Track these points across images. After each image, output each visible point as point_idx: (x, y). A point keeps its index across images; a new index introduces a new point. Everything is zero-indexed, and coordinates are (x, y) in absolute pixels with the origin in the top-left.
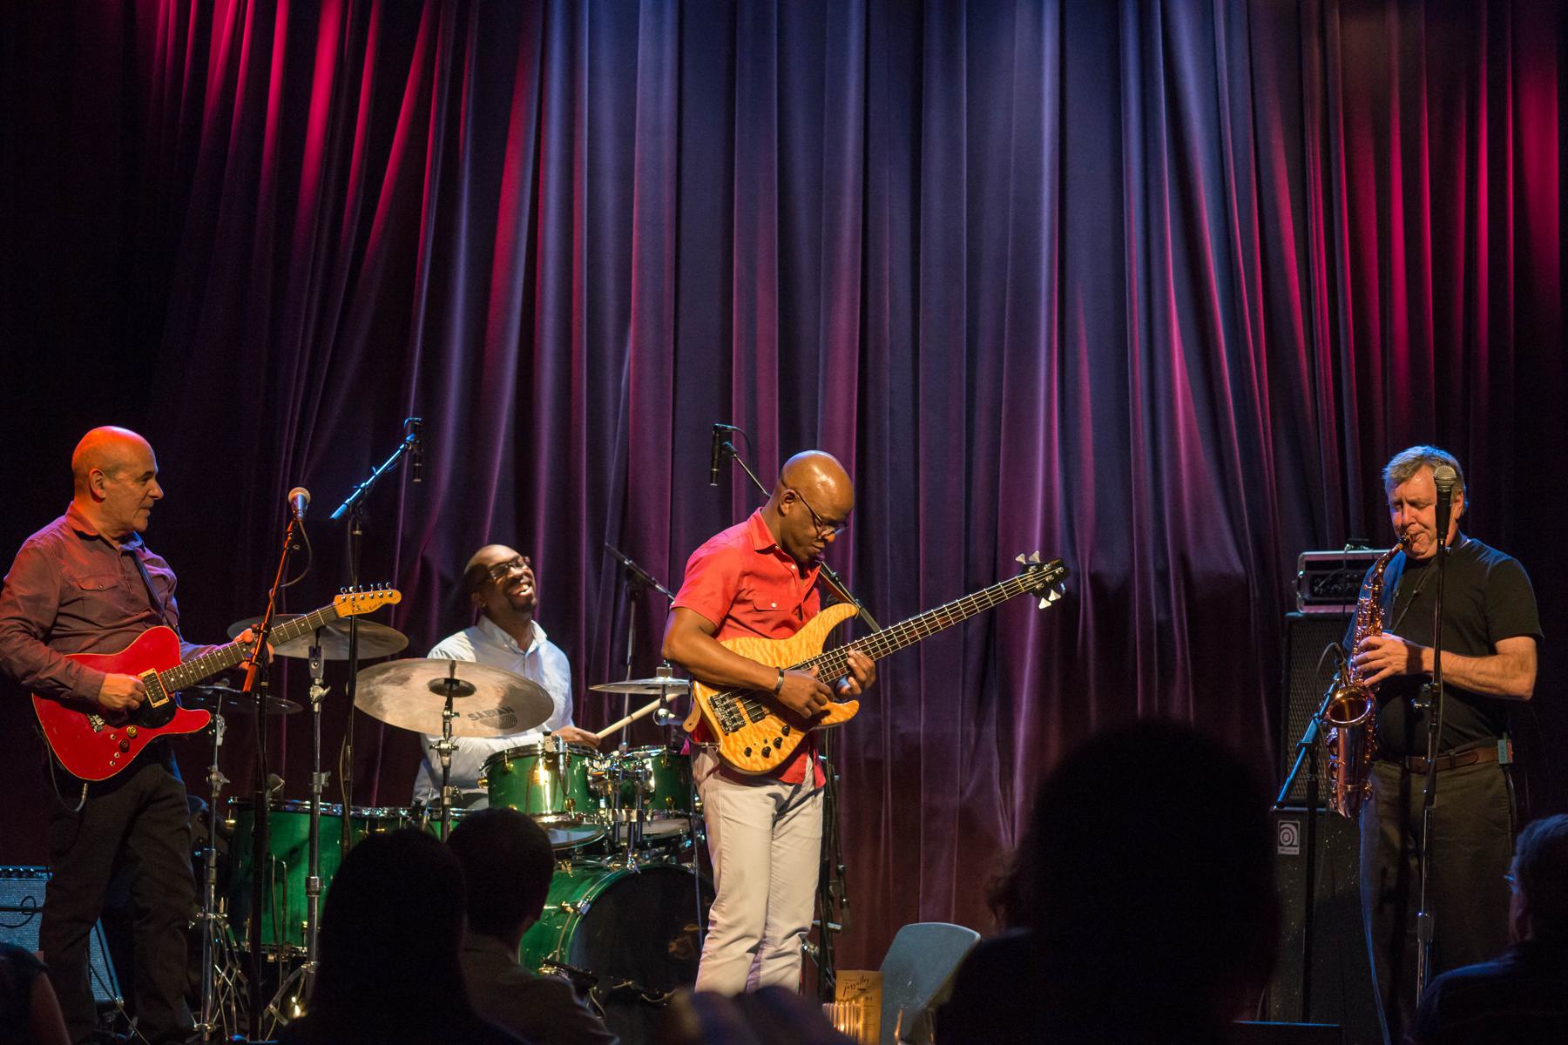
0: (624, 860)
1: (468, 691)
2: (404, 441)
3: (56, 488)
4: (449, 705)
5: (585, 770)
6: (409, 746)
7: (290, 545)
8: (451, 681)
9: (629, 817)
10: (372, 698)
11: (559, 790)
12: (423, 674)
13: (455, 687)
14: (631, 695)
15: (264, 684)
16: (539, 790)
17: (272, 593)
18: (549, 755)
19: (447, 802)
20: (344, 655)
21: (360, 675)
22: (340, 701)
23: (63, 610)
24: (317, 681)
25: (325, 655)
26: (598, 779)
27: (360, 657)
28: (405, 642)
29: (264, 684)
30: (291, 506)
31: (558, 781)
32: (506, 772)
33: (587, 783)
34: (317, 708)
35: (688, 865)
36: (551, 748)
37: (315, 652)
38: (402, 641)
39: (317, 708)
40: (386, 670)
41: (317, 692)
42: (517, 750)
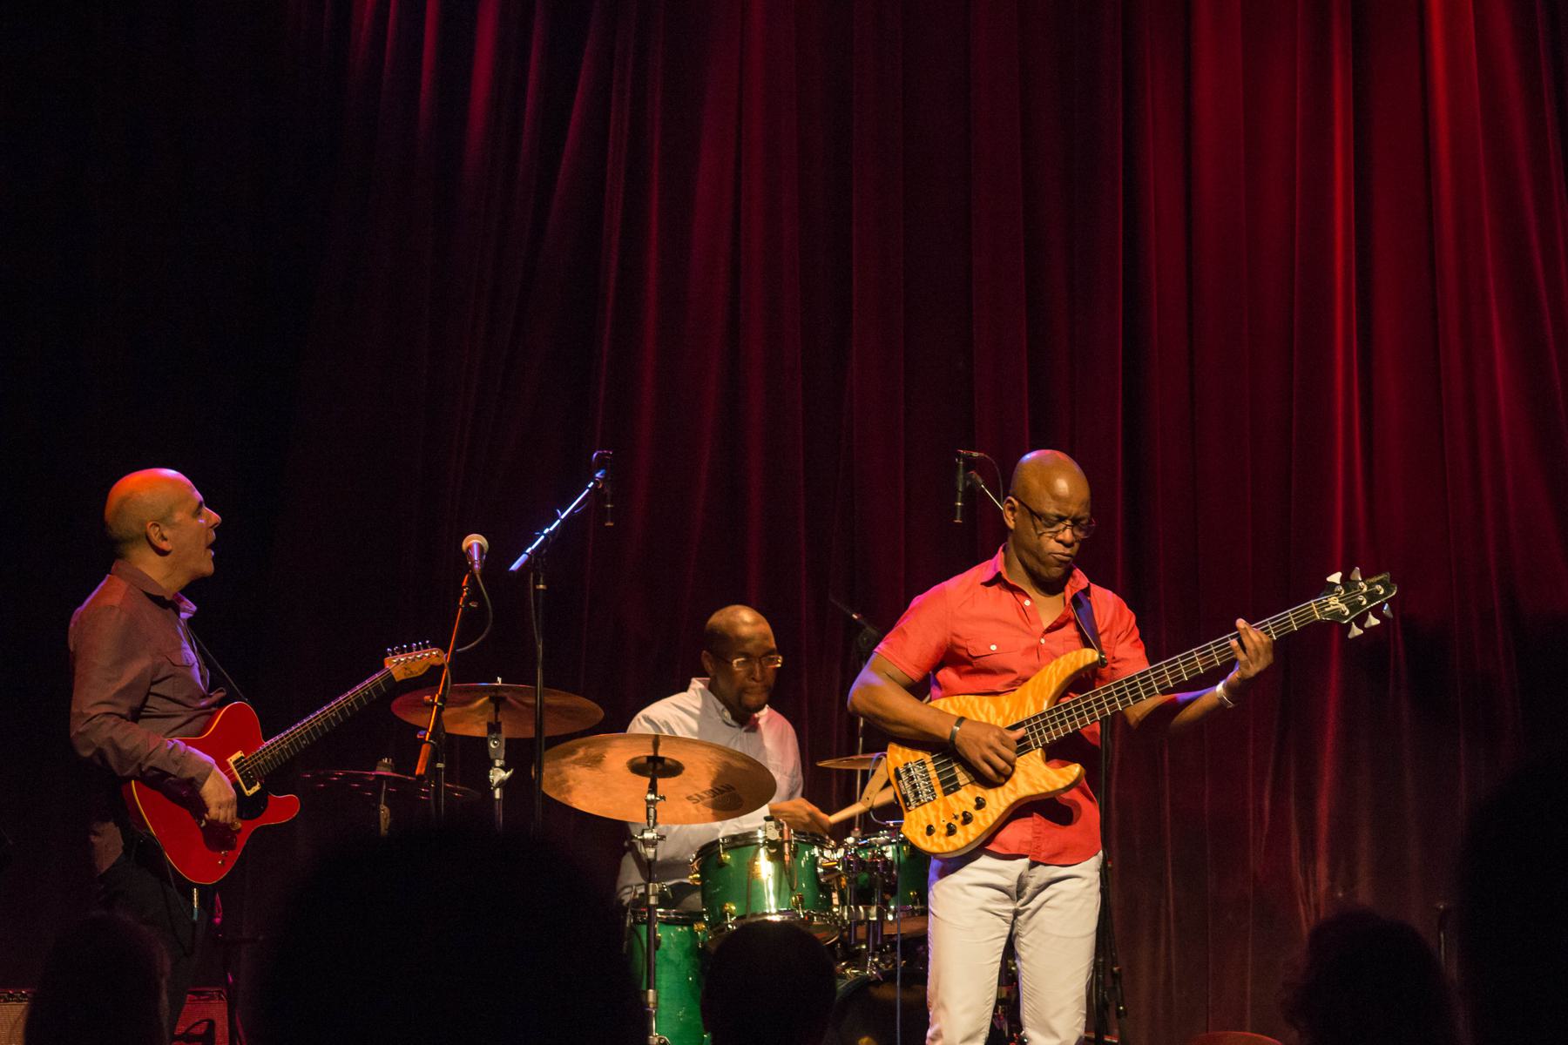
1: (675, 770)
2: (592, 478)
3: (101, 550)
4: (653, 788)
5: (814, 861)
6: (614, 837)
7: (467, 601)
8: (655, 760)
9: (867, 915)
10: (562, 785)
11: (785, 885)
12: (618, 754)
13: (659, 767)
15: (440, 765)
16: (760, 885)
18: (771, 844)
19: (653, 901)
20: (530, 732)
22: (524, 785)
23: (154, 689)
24: (498, 763)
25: (506, 732)
26: (830, 870)
29: (440, 765)
30: (464, 556)
31: (785, 874)
32: (722, 865)
33: (817, 875)
34: (497, 794)
36: (774, 835)
37: (494, 728)
39: (497, 794)
40: (572, 752)
41: (498, 775)
42: (734, 838)
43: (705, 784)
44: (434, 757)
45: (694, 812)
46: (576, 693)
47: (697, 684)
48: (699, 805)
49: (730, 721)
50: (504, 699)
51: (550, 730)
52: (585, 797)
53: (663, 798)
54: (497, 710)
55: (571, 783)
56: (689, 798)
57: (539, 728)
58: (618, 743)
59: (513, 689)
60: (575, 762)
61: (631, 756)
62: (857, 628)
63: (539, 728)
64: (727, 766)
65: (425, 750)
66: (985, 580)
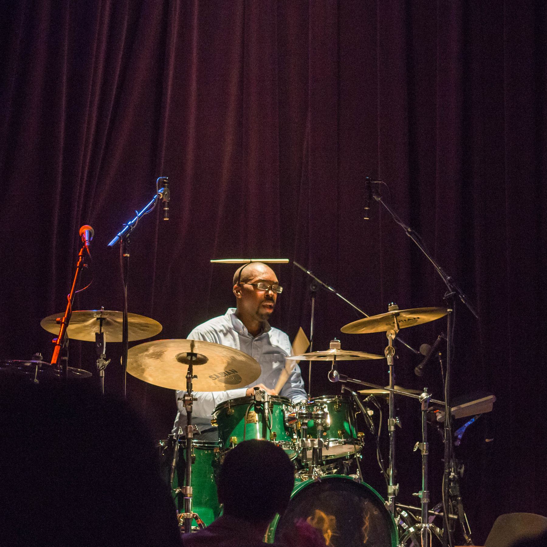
0: (310, 472)
1: (202, 361)
4: (190, 370)
6: (166, 397)
8: (191, 354)
11: (293, 352)
12: (175, 348)
14: (312, 361)
15: (66, 358)
17: (70, 297)
19: (190, 436)
20: (119, 339)
21: (130, 352)
22: (117, 369)
26: (292, 419)
28: (158, 327)
30: (80, 239)
34: (102, 373)
35: (354, 476)
38: (157, 326)
43: (221, 368)
44: (62, 353)
45: (213, 384)
47: (231, 311)
48: (216, 380)
49: (181, 355)
50: (104, 319)
51: (131, 338)
52: (151, 376)
54: (101, 325)
56: (210, 377)
57: (125, 336)
58: (172, 345)
59: (110, 314)
61: (178, 353)
62: (319, 343)
63: (125, 336)
64: (233, 359)
65: (57, 349)
66: (195, 379)
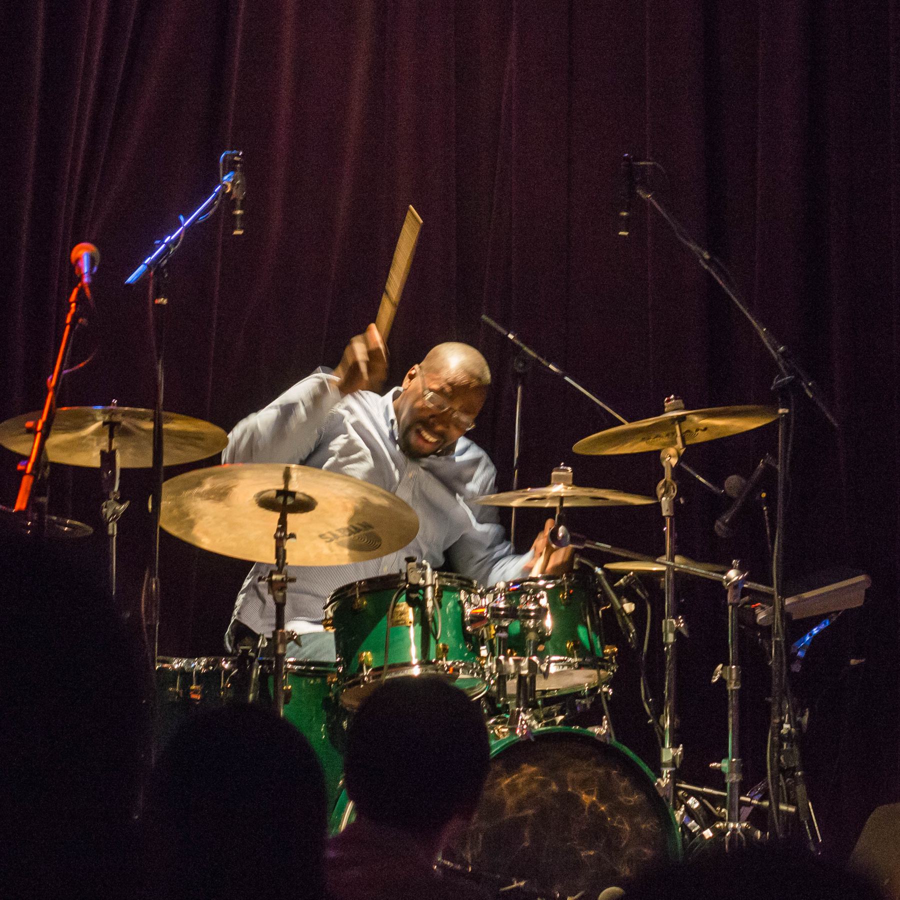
1: (306, 505)
4: (283, 522)
6: (226, 573)
7: (75, 318)
8: (285, 493)
10: (186, 519)
13: (290, 501)
17: (52, 381)
20: (146, 462)
21: (167, 488)
22: (141, 523)
26: (477, 619)
27: (166, 462)
29: (44, 500)
30: (73, 268)
34: (113, 529)
39: (113, 529)
43: (341, 520)
46: (202, 417)
52: (206, 533)
53: (293, 536)
54: (111, 436)
55: (192, 516)
56: (321, 536)
58: (247, 474)
60: (199, 495)
65: (27, 482)
